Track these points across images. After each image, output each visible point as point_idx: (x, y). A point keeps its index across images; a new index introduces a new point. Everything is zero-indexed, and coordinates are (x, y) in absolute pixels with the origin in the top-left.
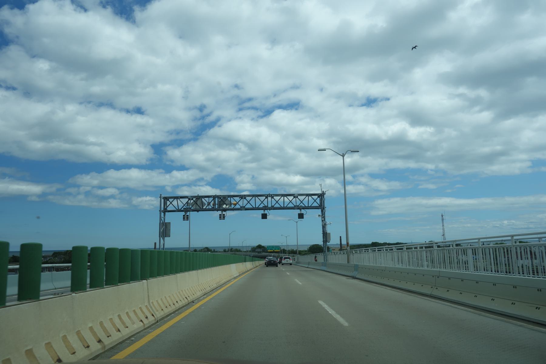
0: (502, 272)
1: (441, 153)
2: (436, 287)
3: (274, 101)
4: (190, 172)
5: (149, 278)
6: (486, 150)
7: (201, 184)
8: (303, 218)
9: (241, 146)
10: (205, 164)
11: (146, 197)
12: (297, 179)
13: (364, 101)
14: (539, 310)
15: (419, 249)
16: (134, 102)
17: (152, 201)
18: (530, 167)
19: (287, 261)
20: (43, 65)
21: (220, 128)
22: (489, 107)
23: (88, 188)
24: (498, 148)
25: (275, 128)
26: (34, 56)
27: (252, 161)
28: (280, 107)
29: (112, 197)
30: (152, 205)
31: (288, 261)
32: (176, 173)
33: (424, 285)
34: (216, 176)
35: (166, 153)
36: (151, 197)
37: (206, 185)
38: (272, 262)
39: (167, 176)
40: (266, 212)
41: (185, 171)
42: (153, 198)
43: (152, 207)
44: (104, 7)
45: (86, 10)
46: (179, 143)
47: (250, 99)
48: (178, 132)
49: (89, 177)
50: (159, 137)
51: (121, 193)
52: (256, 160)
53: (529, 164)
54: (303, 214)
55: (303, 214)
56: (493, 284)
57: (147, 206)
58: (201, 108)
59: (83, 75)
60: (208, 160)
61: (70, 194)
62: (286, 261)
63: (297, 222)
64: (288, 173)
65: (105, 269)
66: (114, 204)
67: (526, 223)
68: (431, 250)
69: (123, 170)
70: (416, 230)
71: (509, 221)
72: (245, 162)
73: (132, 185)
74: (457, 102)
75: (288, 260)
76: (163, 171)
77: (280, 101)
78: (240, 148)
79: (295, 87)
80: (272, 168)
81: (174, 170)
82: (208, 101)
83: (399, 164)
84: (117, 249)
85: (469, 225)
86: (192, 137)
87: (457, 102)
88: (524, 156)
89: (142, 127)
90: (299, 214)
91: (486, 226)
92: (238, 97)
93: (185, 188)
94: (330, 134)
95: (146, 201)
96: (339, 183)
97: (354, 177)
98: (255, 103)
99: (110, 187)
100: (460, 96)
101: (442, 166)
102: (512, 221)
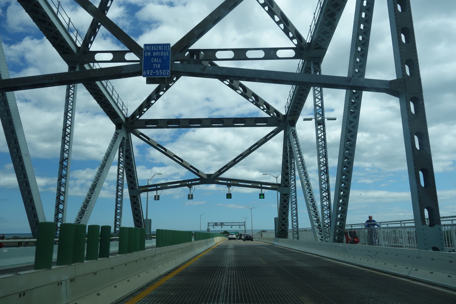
1: (376, 154)
4: (168, 168)
5: (71, 264)
8: (231, 198)
9: (210, 148)
14: (432, 274)
18: (450, 166)
21: (194, 132)
23: (83, 181)
39: (148, 171)
41: (163, 168)
44: (105, 39)
47: (218, 110)
49: (84, 172)
51: (109, 185)
53: (450, 163)
54: (263, 195)
55: (263, 195)
56: (396, 254)
63: (251, 209)
64: (248, 170)
67: (450, 213)
70: (356, 218)
72: (213, 160)
76: (145, 168)
78: (209, 150)
84: (127, 228)
85: (401, 214)
86: (170, 139)
88: (445, 157)
90: (260, 195)
92: (208, 107)
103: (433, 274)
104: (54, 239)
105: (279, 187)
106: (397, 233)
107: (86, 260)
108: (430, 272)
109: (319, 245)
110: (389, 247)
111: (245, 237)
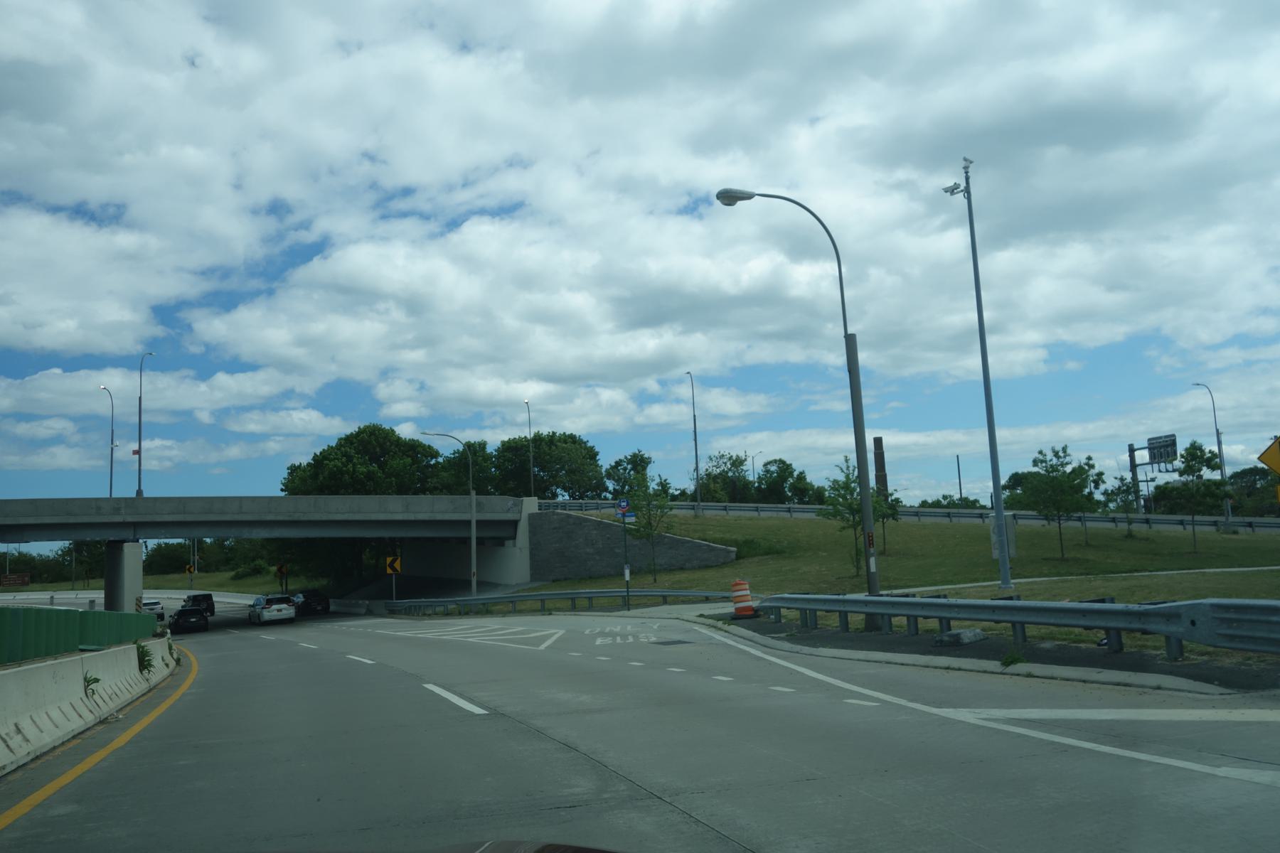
3: (463, 197)
4: (261, 375)
10: (298, 353)
12: (531, 390)
13: (684, 201)
16: (96, 188)
17: (169, 448)
19: (279, 610)
25: (470, 263)
27: (414, 345)
28: (482, 212)
29: (58, 440)
30: (170, 459)
31: (284, 612)
32: (222, 378)
34: (328, 386)
35: (189, 328)
36: (168, 438)
37: (306, 407)
39: (203, 387)
41: (250, 374)
42: (168, 443)
43: (168, 464)
46: (224, 301)
47: (407, 192)
48: (225, 273)
50: (169, 287)
52: (426, 341)
57: (155, 463)
58: (277, 208)
60: (302, 342)
62: (275, 613)
69: (83, 373)
77: (482, 196)
79: (517, 163)
80: (469, 361)
81: (219, 371)
82: (292, 191)
83: (765, 353)
87: (894, 205)
89: (131, 258)
93: (255, 415)
94: (602, 280)
97: (662, 383)
98: (419, 202)
100: (899, 186)
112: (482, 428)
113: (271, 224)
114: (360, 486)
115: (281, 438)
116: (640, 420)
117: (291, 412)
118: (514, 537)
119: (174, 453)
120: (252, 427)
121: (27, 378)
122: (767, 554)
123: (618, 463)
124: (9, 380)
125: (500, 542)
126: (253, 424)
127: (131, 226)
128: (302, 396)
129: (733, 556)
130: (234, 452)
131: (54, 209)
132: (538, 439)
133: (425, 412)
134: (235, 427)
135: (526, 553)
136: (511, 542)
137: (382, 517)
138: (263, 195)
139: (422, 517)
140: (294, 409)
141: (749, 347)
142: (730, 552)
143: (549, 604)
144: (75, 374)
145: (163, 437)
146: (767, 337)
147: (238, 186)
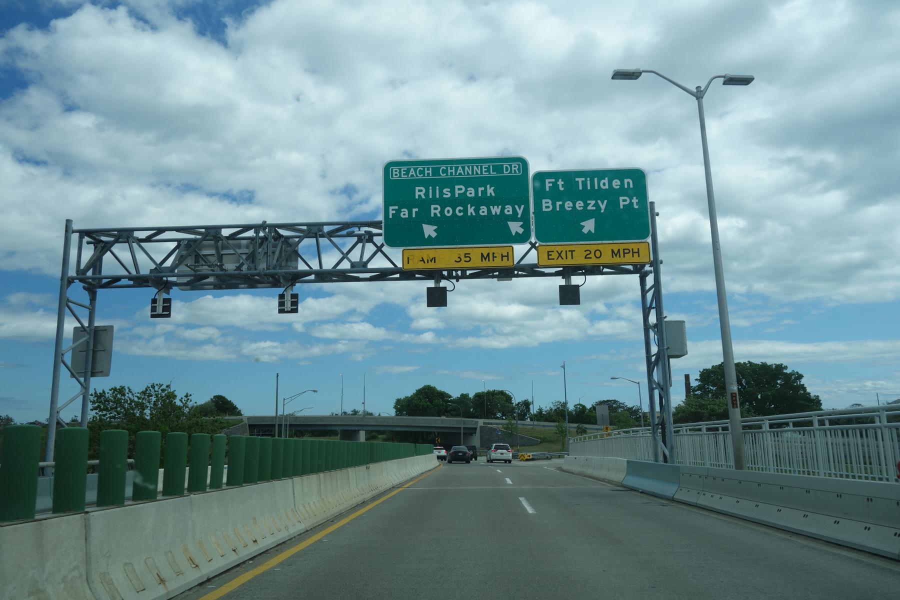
0: (841, 471)
1: (756, 264)
2: (703, 492)
4: (335, 300)
6: (836, 259)
7: (354, 319)
11: (265, 342)
15: (705, 432)
16: (237, 181)
17: (275, 347)
19: (502, 454)
20: (83, 121)
22: (842, 182)
24: (857, 255)
26: (70, 108)
29: (209, 341)
30: (275, 355)
33: (872, 526)
34: (378, 306)
37: (363, 321)
38: (460, 454)
40: (576, 280)
41: (327, 299)
42: (275, 344)
43: (274, 358)
45: (154, 28)
56: (836, 494)
57: (267, 357)
59: (150, 136)
61: (139, 337)
62: (499, 455)
65: (225, 471)
66: (212, 353)
68: (725, 433)
71: (875, 382)
73: (237, 320)
74: (784, 174)
75: (504, 451)
81: (308, 297)
87: (784, 174)
91: (835, 390)
93: (330, 327)
95: (263, 348)
96: (585, 316)
97: (608, 306)
99: (205, 326)
100: (789, 161)
101: (760, 286)
102: (880, 382)
103: (864, 527)
104: (87, 462)
105: (794, 187)
106: (637, 431)
107: (210, 489)
108: (894, 534)
109: (700, 477)
110: (813, 475)
111: (453, 453)
112: (479, 336)
113: (343, 201)
114: (424, 412)
115: (346, 342)
116: (591, 332)
117: (353, 325)
118: (475, 433)
119: (279, 350)
120: (329, 334)
121: (194, 302)
122: (549, 442)
123: (519, 403)
124: (182, 303)
125: (471, 434)
126: (328, 332)
127: (260, 204)
128: (361, 314)
129: (539, 442)
130: (316, 350)
131: (211, 195)
132: (489, 393)
133: (441, 325)
134: (317, 334)
135: (479, 439)
136: (474, 435)
137: (435, 425)
138: (341, 183)
139: (447, 425)
140: (355, 322)
141: (672, 279)
142: (538, 441)
143: (482, 454)
144: (222, 298)
145: (272, 340)
146: (687, 272)
147: (324, 176)
